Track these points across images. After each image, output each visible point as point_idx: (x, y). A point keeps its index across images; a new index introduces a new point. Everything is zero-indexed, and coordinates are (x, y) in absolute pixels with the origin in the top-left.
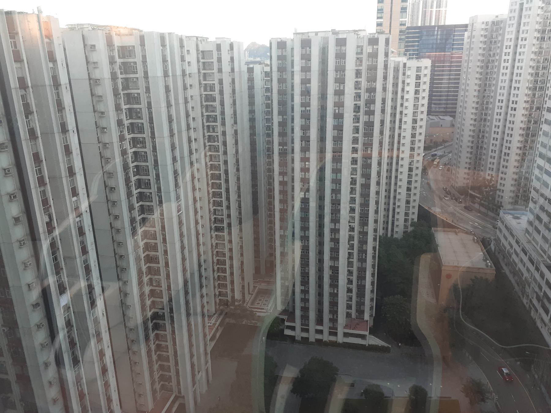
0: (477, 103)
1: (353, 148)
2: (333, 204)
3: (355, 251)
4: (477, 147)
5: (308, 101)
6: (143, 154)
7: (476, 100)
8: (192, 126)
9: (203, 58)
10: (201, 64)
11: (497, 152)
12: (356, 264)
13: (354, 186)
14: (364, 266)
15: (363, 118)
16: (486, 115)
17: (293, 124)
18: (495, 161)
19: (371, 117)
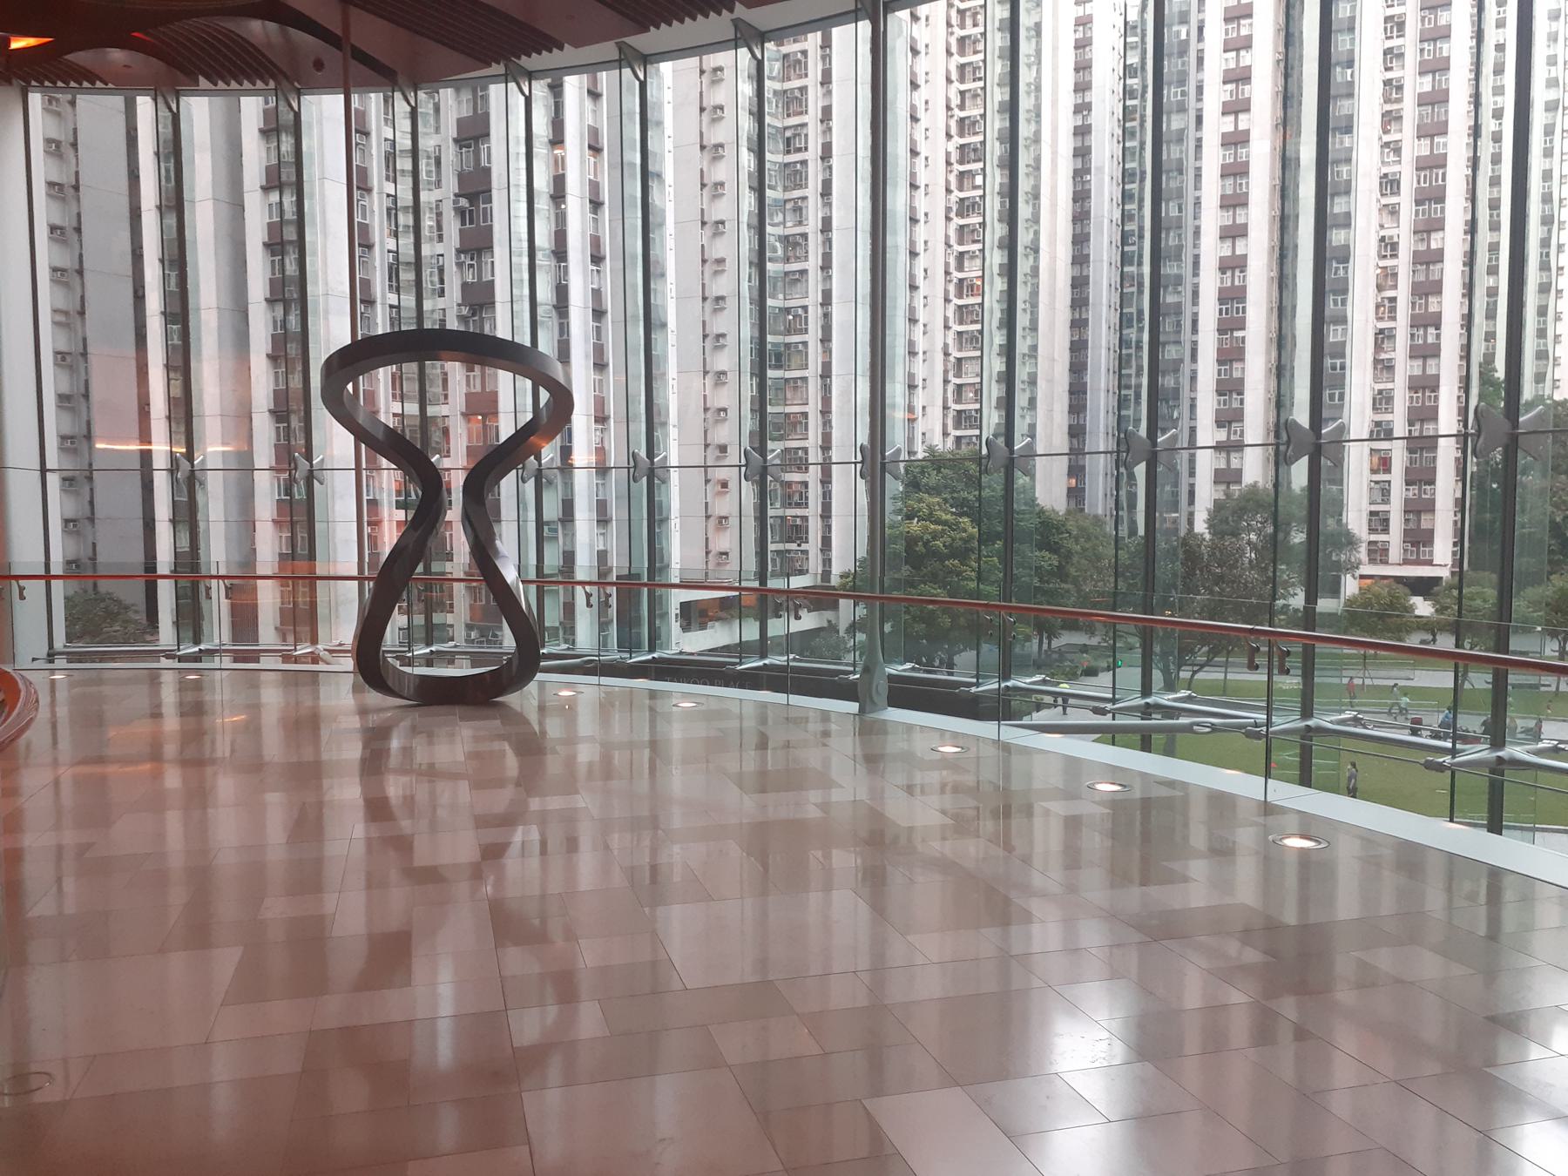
1: (1372, 513)
3: (1402, 325)
5: (1235, 405)
6: (797, 93)
8: (920, 348)
9: (962, 107)
10: (950, 388)
12: (1405, 368)
13: (1395, 107)
14: (1431, 371)
15: (1414, 149)
17: (1197, 194)
19: (1431, 362)
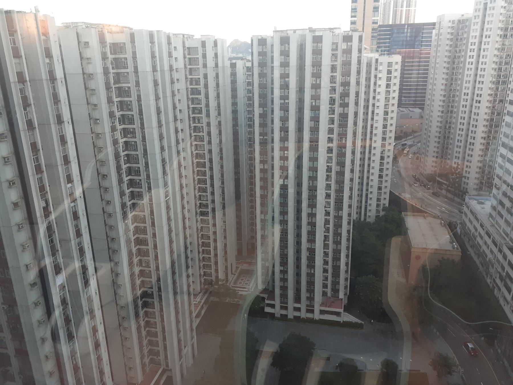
0: (444, 96)
1: (329, 138)
2: (310, 190)
3: (331, 234)
4: (445, 137)
5: (286, 94)
6: (133, 143)
7: (443, 93)
8: (179, 117)
9: (189, 54)
10: (187, 60)
11: (463, 142)
12: (331, 246)
13: (329, 174)
14: (339, 248)
15: (338, 110)
16: (452, 107)
17: (272, 116)
18: (461, 150)
19: (346, 109)
